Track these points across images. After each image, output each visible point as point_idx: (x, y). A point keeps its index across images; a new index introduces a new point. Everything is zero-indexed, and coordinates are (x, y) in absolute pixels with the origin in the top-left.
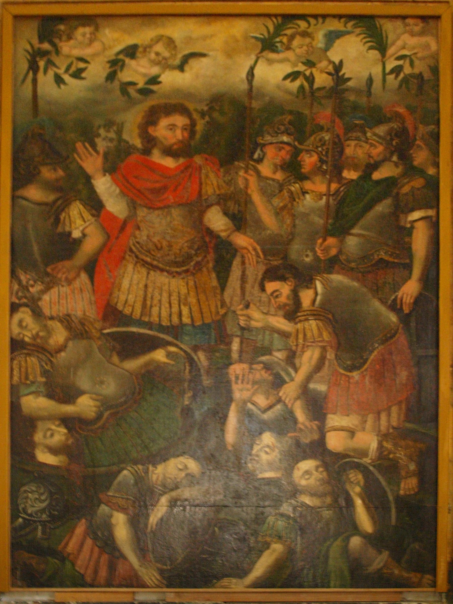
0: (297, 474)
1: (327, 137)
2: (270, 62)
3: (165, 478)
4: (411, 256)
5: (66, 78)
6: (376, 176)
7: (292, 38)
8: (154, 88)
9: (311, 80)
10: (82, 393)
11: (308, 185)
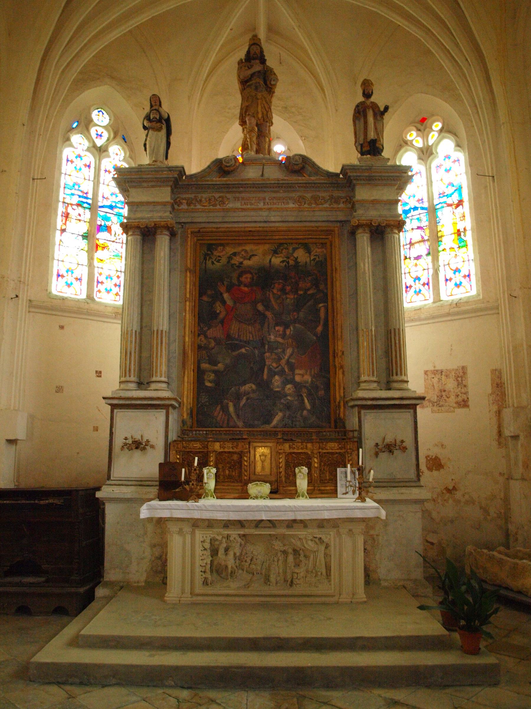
0: (286, 389)
1: (293, 280)
2: (276, 257)
3: (245, 391)
4: (320, 318)
5: (215, 262)
6: (309, 292)
7: (282, 250)
8: (242, 265)
9: (288, 263)
10: (219, 363)
11: (288, 296)
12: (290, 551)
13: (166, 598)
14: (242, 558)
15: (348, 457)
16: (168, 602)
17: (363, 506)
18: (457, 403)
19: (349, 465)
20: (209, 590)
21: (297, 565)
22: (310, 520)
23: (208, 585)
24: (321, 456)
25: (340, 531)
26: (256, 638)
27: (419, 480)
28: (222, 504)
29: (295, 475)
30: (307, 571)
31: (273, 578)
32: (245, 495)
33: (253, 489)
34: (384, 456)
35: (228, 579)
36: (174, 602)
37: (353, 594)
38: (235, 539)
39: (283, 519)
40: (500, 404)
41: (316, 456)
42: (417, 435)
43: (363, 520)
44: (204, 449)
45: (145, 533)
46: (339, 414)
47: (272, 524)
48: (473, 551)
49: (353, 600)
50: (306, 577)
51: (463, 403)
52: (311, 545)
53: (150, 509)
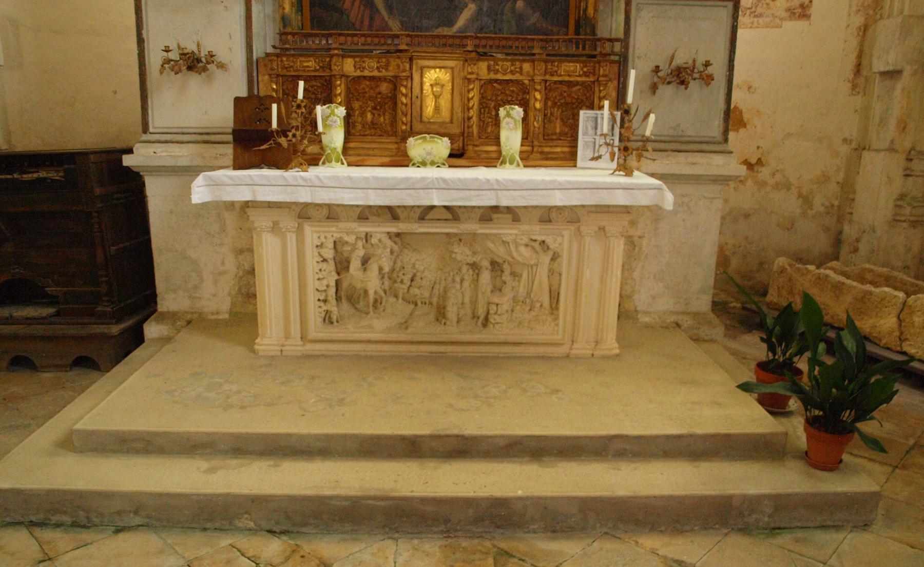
12: (486, 263)
13: (256, 347)
15: (600, 91)
16: (261, 353)
17: (632, 184)
18: (788, 10)
19: (606, 103)
20: (334, 332)
21: (498, 289)
22: (525, 207)
23: (332, 323)
24: (548, 88)
25: (582, 228)
26: (416, 436)
27: (726, 140)
28: (352, 175)
29: (497, 124)
30: (515, 300)
31: (452, 312)
32: (402, 160)
33: (416, 147)
34: (666, 91)
35: (367, 313)
36: (272, 353)
37: (597, 342)
38: (380, 241)
39: (473, 204)
40: (871, 12)
41: (538, 87)
42: (734, 53)
43: (626, 210)
44: (324, 71)
45: (223, 230)
46: (586, 10)
47: (452, 213)
48: (788, 267)
49: (596, 353)
50: (512, 311)
51: (800, 10)
52: (524, 254)
53: (214, 184)
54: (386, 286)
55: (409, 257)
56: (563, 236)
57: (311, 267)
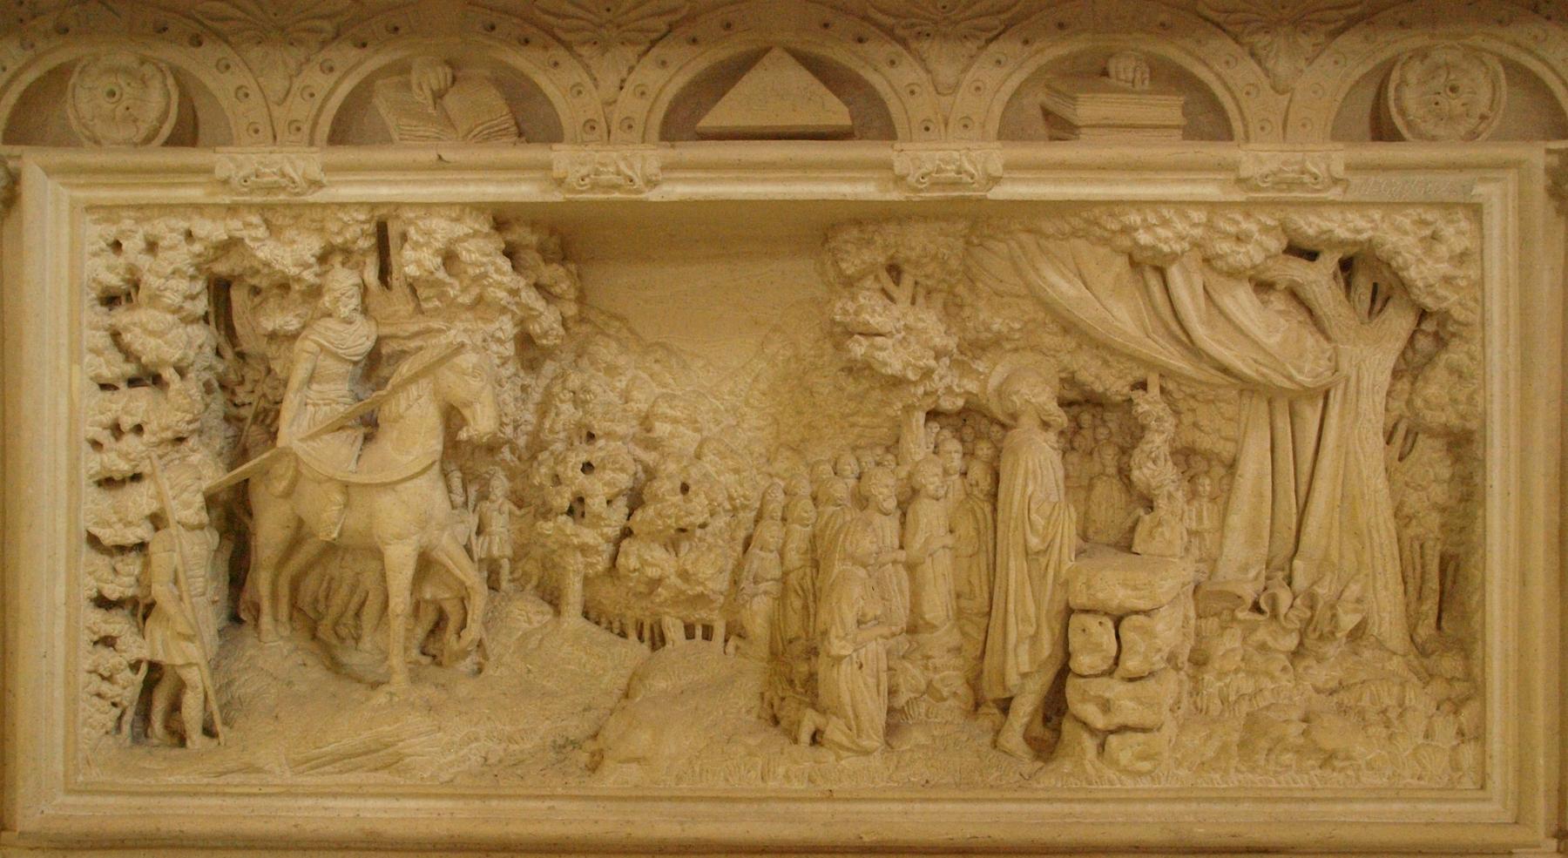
14: (541, 475)
38: (449, 258)
50: (1199, 661)
54: (499, 543)
55: (621, 384)
56: (1476, 211)
57: (63, 408)
